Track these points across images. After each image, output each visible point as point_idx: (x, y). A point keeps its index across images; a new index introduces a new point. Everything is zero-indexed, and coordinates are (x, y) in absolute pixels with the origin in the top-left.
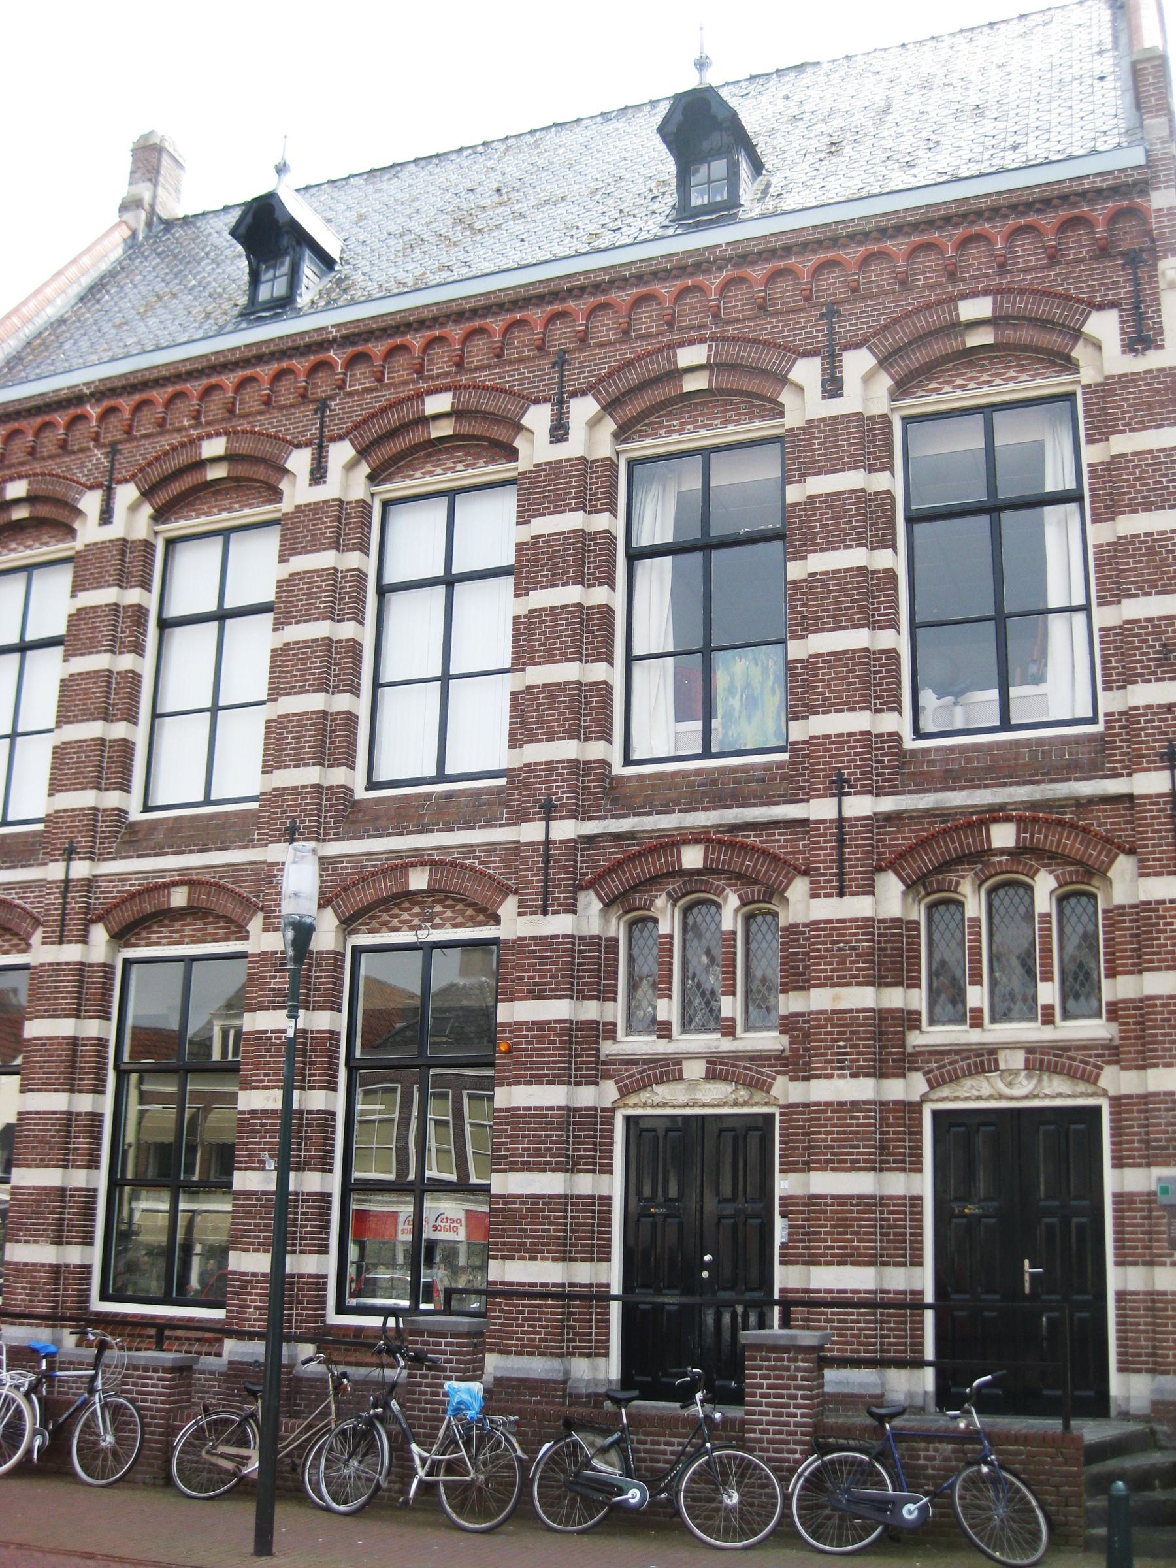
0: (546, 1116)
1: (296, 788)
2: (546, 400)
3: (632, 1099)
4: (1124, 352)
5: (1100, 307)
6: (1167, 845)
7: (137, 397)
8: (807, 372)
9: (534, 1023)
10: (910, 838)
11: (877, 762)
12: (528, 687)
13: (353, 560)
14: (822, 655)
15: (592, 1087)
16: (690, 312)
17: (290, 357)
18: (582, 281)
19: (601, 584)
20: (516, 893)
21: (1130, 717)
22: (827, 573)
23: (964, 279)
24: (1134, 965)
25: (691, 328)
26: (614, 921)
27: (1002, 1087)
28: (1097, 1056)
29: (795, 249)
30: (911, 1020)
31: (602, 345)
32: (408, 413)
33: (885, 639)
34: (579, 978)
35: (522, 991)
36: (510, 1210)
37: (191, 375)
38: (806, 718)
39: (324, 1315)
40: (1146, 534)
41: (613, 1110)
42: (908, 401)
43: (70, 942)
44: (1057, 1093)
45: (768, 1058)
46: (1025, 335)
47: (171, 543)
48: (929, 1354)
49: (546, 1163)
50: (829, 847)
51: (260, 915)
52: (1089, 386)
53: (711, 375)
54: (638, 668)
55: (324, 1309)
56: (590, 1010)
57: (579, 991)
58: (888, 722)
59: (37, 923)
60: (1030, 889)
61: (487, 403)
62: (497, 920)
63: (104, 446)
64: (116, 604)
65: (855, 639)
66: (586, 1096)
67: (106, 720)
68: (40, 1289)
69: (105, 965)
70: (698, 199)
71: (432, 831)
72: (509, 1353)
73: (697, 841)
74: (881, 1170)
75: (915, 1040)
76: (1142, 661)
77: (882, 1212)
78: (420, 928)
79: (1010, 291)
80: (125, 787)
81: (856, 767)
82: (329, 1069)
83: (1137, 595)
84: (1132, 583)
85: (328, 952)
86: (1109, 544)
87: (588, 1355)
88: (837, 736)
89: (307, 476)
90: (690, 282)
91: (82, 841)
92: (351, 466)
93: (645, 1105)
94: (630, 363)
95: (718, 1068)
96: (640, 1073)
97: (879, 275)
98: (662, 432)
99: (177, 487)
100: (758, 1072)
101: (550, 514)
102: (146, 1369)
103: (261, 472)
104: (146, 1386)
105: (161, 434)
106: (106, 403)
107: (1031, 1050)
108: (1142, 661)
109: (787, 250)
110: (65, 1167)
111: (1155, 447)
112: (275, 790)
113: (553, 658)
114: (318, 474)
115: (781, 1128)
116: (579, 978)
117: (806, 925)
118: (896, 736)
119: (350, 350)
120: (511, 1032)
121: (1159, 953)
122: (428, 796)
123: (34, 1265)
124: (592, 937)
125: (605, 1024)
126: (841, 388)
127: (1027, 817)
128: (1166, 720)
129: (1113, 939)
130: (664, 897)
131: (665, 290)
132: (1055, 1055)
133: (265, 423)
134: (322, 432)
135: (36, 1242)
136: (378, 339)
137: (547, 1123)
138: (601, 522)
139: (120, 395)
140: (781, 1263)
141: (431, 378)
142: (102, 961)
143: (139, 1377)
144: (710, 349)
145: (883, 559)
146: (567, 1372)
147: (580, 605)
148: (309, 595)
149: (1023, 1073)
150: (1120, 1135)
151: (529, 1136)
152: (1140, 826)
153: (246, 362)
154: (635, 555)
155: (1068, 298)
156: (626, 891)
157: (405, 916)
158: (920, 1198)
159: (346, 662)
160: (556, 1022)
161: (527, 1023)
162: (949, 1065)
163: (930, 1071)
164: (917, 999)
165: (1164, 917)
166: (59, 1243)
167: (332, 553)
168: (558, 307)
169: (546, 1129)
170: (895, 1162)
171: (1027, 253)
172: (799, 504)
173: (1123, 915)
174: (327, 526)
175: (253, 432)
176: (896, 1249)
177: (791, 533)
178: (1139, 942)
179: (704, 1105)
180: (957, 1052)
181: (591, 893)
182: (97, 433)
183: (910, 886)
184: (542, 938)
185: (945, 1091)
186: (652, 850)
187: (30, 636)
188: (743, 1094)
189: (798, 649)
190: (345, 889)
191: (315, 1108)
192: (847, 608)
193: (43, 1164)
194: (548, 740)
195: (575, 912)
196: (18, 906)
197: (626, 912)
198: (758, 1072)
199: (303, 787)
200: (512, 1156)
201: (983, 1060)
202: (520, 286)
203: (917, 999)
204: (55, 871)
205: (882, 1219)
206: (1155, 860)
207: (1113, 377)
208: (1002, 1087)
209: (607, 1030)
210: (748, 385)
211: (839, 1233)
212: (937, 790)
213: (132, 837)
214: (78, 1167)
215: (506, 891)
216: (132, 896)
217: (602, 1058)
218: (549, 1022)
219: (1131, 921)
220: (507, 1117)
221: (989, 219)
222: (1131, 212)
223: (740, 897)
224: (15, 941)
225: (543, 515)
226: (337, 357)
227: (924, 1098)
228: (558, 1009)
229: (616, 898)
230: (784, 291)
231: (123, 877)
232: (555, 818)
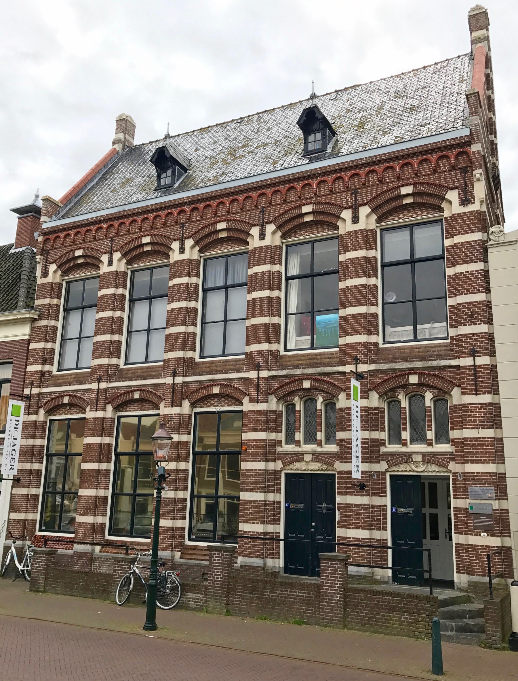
0: (258, 473)
1: (175, 358)
2: (258, 225)
3: (287, 468)
4: (460, 205)
5: (452, 189)
6: (472, 384)
7: (120, 221)
8: (347, 214)
9: (254, 440)
10: (381, 379)
11: (369, 352)
12: (252, 325)
13: (194, 280)
14: (350, 315)
15: (273, 463)
16: (307, 193)
17: (172, 208)
18: (270, 182)
19: (276, 290)
20: (248, 395)
21: (459, 337)
22: (352, 286)
23: (403, 179)
24: (460, 426)
25: (307, 199)
26: (281, 405)
27: (414, 467)
28: (448, 458)
29: (343, 170)
30: (382, 443)
31: (277, 205)
32: (212, 229)
33: (373, 309)
34: (269, 425)
35: (250, 429)
36: (246, 505)
37: (138, 214)
38: (345, 337)
39: (184, 542)
40: (466, 272)
41: (281, 471)
42: (383, 224)
43: (99, 410)
44: (433, 470)
45: (333, 454)
46: (424, 199)
48: (390, 565)
49: (258, 489)
51: (164, 402)
52: (447, 217)
53: (314, 215)
55: (184, 539)
56: (273, 436)
57: (269, 429)
58: (373, 339)
59: (88, 404)
60: (424, 397)
61: (238, 226)
62: (242, 404)
63: (109, 238)
64: (114, 294)
65: (362, 309)
66: (271, 466)
67: (111, 334)
68: (88, 532)
69: (111, 418)
70: (311, 147)
71: (221, 373)
72: (245, 556)
73: (308, 379)
74: (372, 496)
75: (383, 450)
76: (463, 318)
77: (372, 511)
78: (217, 406)
79: (419, 183)
80: (119, 357)
81: (362, 354)
82: (186, 455)
83: (462, 294)
84: (460, 290)
85: (186, 414)
86: (453, 275)
87: (273, 558)
88: (355, 343)
89: (178, 251)
90: (306, 182)
91: (104, 376)
92: (193, 247)
93: (291, 470)
94: (286, 212)
96: (290, 458)
97: (373, 178)
98: (297, 235)
99: (134, 253)
100: (329, 459)
101: (259, 265)
102: (122, 562)
103: (162, 249)
104: (122, 568)
105: (129, 234)
106: (109, 223)
107: (424, 454)
108: (463, 318)
109: (341, 170)
110: (97, 489)
111: (470, 240)
112: (169, 359)
114: (182, 250)
115: (337, 479)
116: (269, 425)
117: (345, 408)
119: (192, 206)
120: (246, 443)
121: (469, 422)
122: (220, 361)
123: (86, 523)
124: (273, 411)
125: (278, 441)
126: (358, 220)
127: (421, 373)
128: (472, 339)
129: (453, 416)
130: (297, 397)
131: (298, 185)
132: (432, 457)
133: (163, 232)
134: (183, 235)
135: (87, 515)
136: (201, 202)
137: (259, 475)
138: (276, 268)
139: (113, 220)
140: (338, 527)
141: (219, 216)
142: (110, 417)
143: (119, 565)
144: (313, 207)
145: (372, 281)
146: (265, 564)
147: (269, 297)
148: (179, 292)
149: (421, 463)
150: (456, 487)
151: (252, 479)
152: (462, 377)
153: (157, 210)
154: (288, 279)
155: (440, 186)
156: (285, 395)
157: (212, 402)
158: (386, 506)
159: (192, 315)
160: (261, 440)
161: (252, 440)
162: (395, 459)
163: (389, 461)
164: (384, 435)
165: (471, 410)
166: (95, 516)
167: (187, 278)
168: (262, 191)
169: (258, 477)
170: (376, 493)
171: (426, 169)
172: (343, 261)
173: (456, 408)
174: (185, 268)
175: (160, 235)
176: (377, 524)
177: (340, 271)
178: (462, 418)
179: (311, 470)
180: (398, 455)
181: (273, 395)
182: (106, 233)
183: (381, 396)
184: (257, 411)
185: (394, 468)
186: (293, 381)
188: (325, 467)
189: (342, 313)
190: (192, 393)
191: (181, 468)
192: (359, 299)
193: (89, 487)
194: (259, 343)
195: (268, 402)
196: (82, 398)
197: (285, 402)
198: (329, 459)
199: (178, 358)
200: (247, 486)
201: (407, 457)
202: (249, 184)
203: (384, 435)
204: (94, 386)
205: (372, 513)
206: (467, 389)
207: (455, 214)
208: (414, 467)
209: (279, 443)
210: (326, 220)
211: (357, 518)
212: (390, 363)
213: (117, 373)
214: (101, 489)
215: (245, 395)
216: (121, 395)
217: (277, 453)
218: (259, 440)
219: (459, 410)
220: (245, 473)
221: (412, 157)
223: (323, 398)
224: (81, 410)
225: (257, 265)
226: (187, 209)
227: (387, 470)
228: (262, 436)
229: (281, 397)
230: (339, 185)
231: (118, 388)
232: (261, 370)
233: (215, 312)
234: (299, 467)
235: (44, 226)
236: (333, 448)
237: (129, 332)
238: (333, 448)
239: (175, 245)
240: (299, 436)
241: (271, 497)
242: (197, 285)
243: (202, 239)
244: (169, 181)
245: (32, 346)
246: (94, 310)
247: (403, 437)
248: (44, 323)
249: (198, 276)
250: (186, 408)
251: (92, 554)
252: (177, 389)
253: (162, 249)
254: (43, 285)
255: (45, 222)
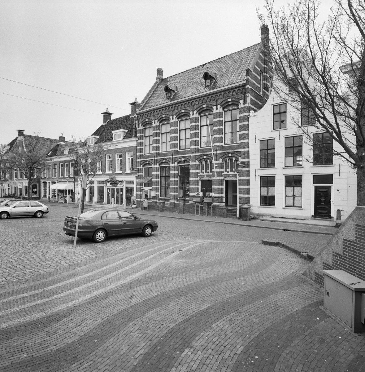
32: (180, 112)
47: (161, 125)
50: (192, 158)
54: (226, 134)
59: (190, 160)
61: (187, 111)
66: (197, 179)
70: (207, 85)
95: (208, 176)
97: (221, 97)
107: (232, 175)
109: (212, 94)
113: (217, 134)
114: (217, 109)
118: (198, 148)
153: (188, 101)
187: (167, 132)
222: (244, 88)
227: (224, 179)
233: (183, 137)
234: (203, 179)
235: (137, 112)
236: (211, 174)
237: (161, 143)
238: (211, 174)
239: (214, 107)
240: (229, 170)
241: (221, 187)
242: (222, 121)
243: (223, 105)
244: (209, 84)
245: (137, 148)
246: (152, 137)
247: (208, 171)
248: (139, 141)
249: (222, 118)
250: (158, 166)
251: (174, 202)
252: (194, 157)
253: (168, 118)
254: (138, 130)
255: (137, 111)
